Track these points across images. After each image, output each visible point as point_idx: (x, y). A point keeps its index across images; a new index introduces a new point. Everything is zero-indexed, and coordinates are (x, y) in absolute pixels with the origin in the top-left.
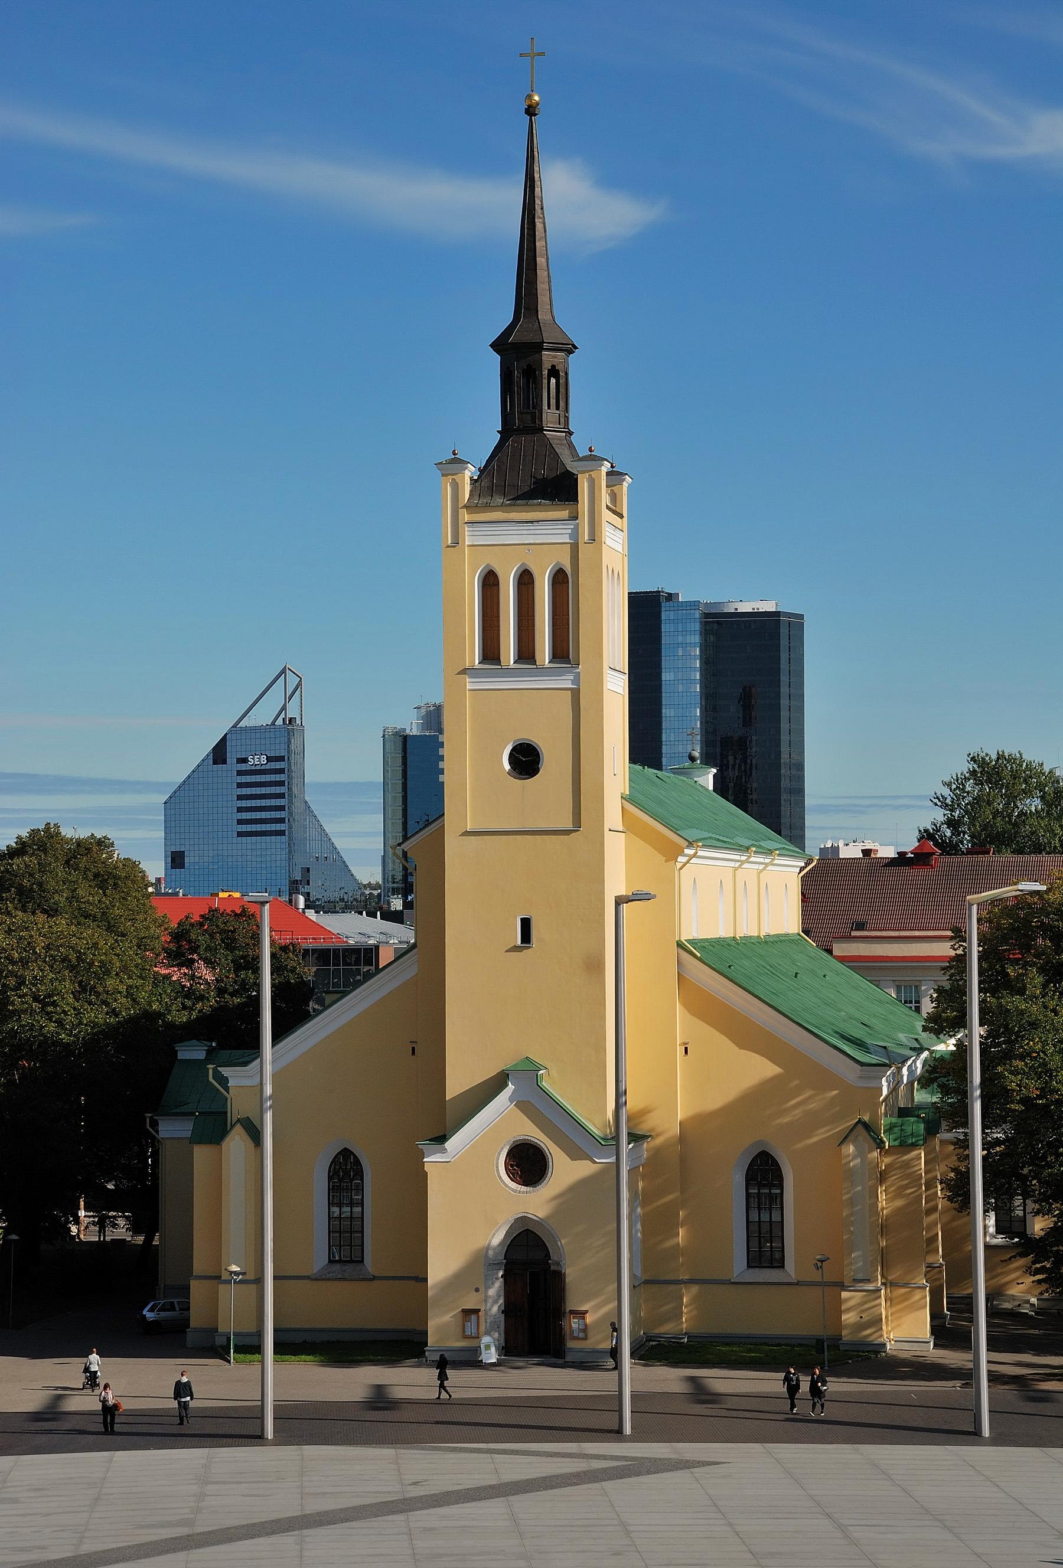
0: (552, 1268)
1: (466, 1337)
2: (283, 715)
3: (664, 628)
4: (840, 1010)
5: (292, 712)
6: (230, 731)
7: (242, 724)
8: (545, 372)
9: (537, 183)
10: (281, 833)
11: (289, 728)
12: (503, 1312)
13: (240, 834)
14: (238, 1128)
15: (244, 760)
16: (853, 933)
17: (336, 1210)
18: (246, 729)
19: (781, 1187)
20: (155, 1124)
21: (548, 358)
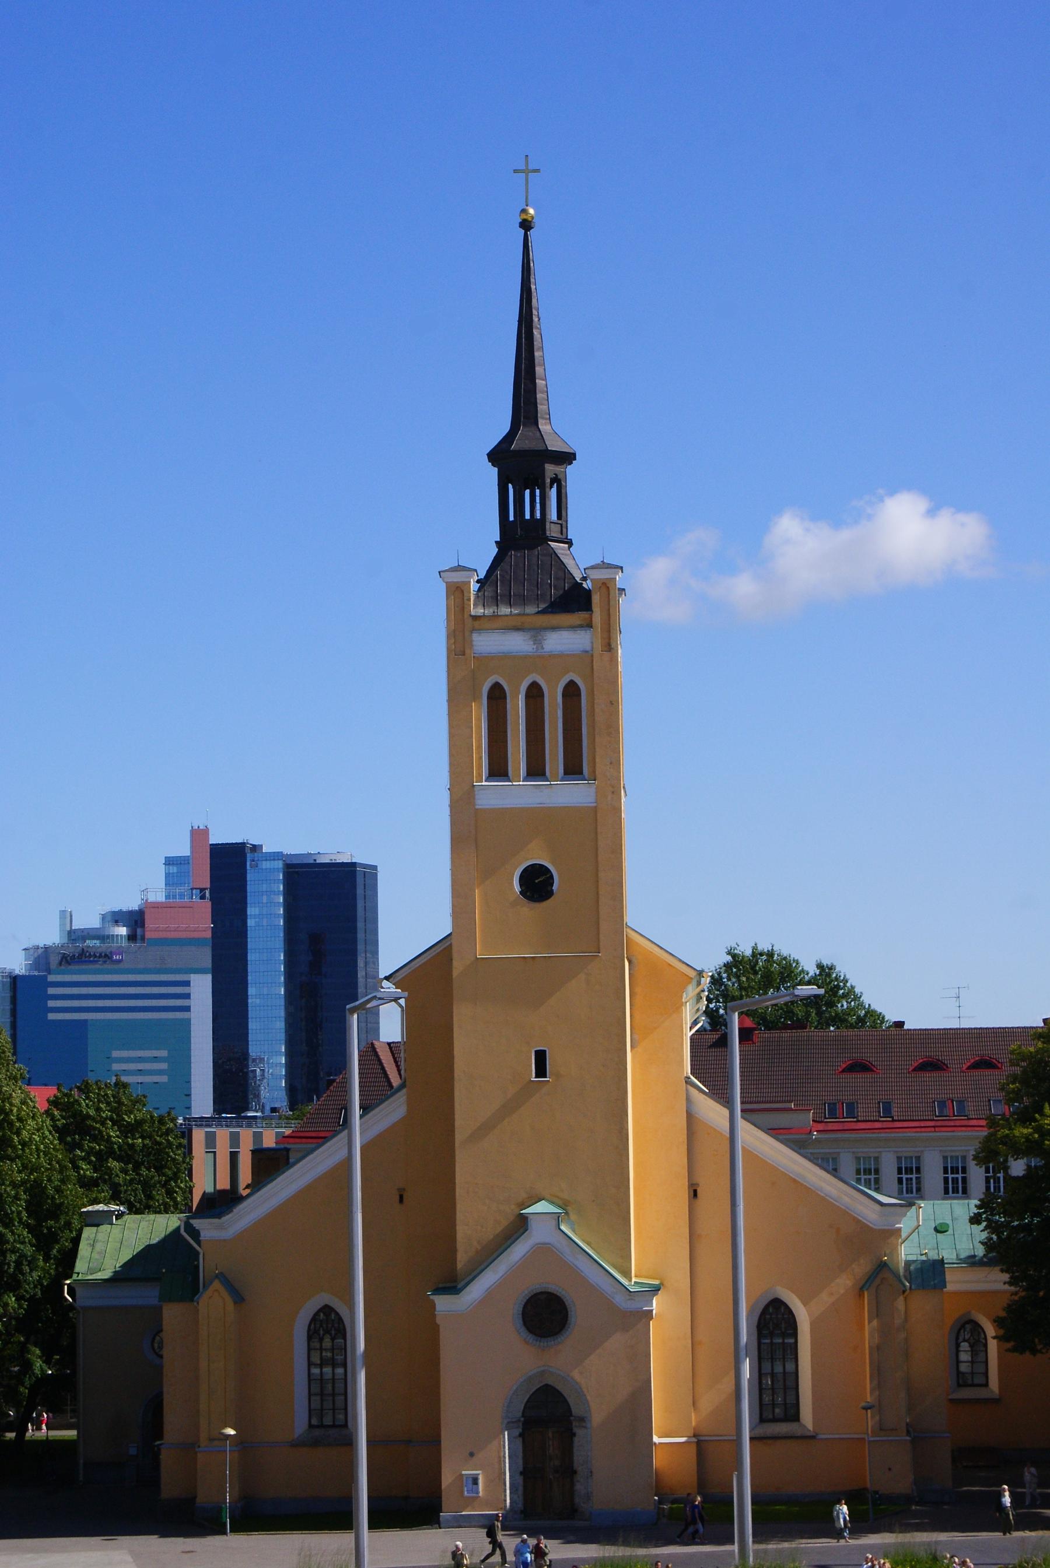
8: (548, 481)
9: (534, 294)
12: (521, 1473)
14: (216, 1284)
17: (316, 1371)
19: (795, 1334)
21: (550, 469)
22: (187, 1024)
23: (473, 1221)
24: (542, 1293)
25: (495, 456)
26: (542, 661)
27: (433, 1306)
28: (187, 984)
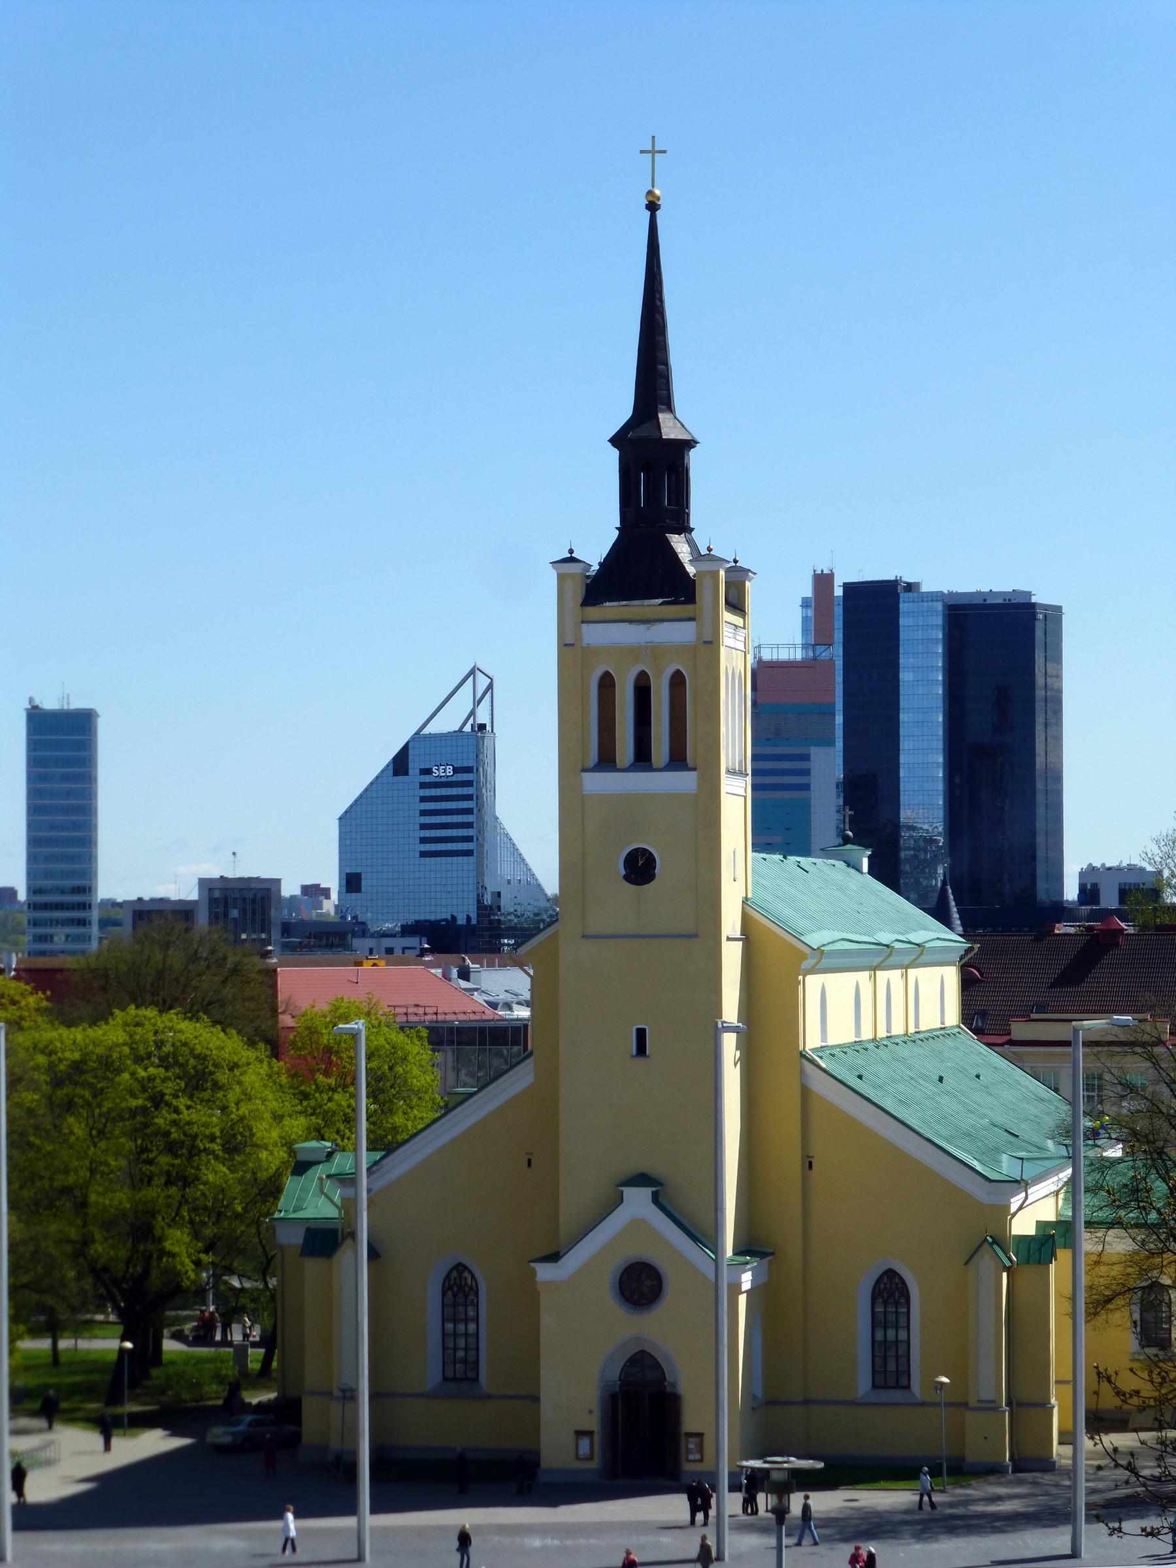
0: (668, 1389)
1: (578, 1458)
2: (471, 721)
3: (903, 621)
4: (984, 1116)
5: (483, 717)
6: (413, 739)
7: (426, 731)
10: (469, 853)
13: (424, 854)
15: (428, 771)
16: (1033, 1016)
18: (431, 736)
22: (806, 807)
23: (579, 1175)
24: (637, 1263)
25: (617, 440)
26: (656, 651)
27: (533, 1273)
28: (806, 757)
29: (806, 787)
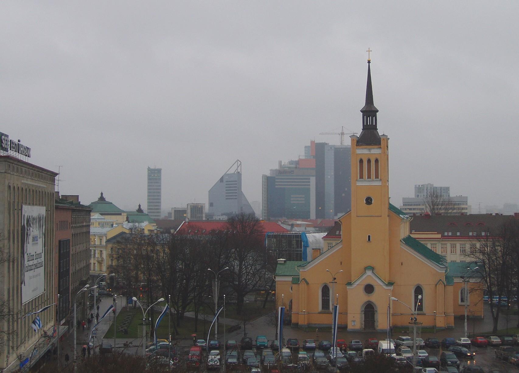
5: (239, 170)
10: (236, 199)
11: (239, 174)
20: (275, 278)
22: (309, 190)
28: (309, 179)
29: (309, 185)
